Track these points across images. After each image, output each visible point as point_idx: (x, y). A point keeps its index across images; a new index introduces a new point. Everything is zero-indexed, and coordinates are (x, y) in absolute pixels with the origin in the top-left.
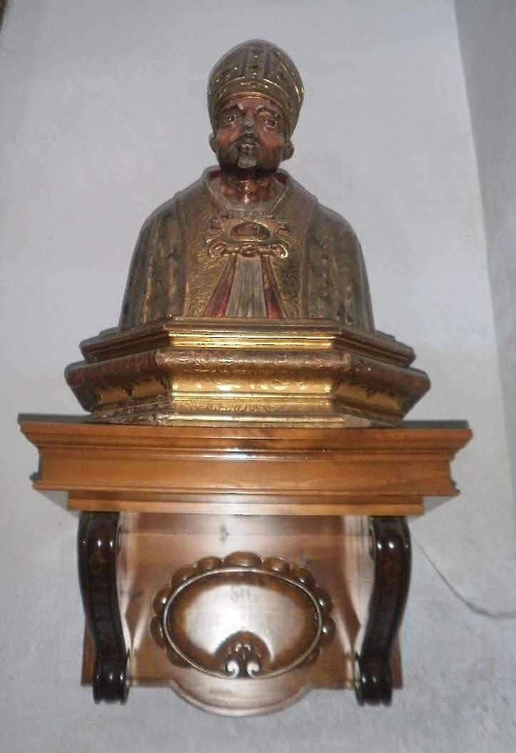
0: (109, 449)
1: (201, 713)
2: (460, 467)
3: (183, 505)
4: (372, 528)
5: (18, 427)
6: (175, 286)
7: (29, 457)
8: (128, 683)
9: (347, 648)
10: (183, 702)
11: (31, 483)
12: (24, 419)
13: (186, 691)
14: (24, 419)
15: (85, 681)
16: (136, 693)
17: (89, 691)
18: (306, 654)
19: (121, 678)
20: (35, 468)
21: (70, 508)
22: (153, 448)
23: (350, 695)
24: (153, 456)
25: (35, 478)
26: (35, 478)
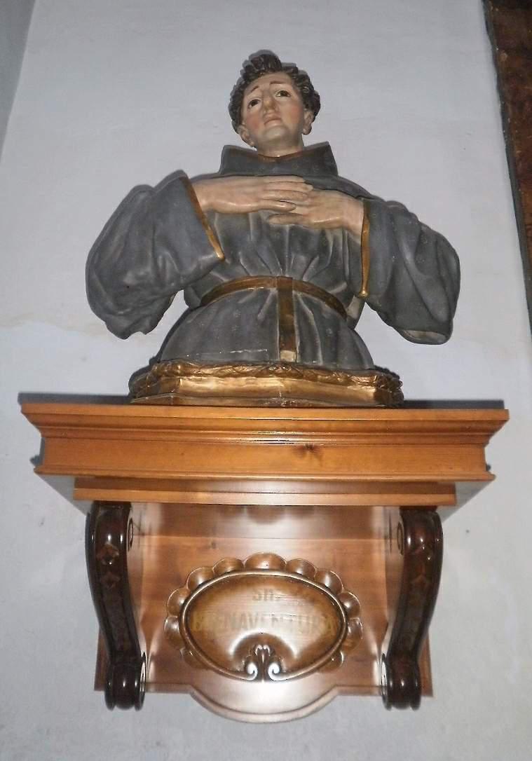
0: (182, 433)
1: (216, 717)
2: (496, 450)
3: (226, 495)
4: (401, 522)
5: (19, 408)
6: (278, 222)
7: (31, 440)
8: (142, 689)
9: (374, 649)
10: (210, 714)
11: (32, 467)
12: (25, 399)
13: (212, 702)
14: (25, 399)
15: (97, 687)
16: (152, 699)
17: (101, 695)
18: (328, 656)
19: (136, 684)
20: (36, 450)
21: (76, 500)
22: (477, 434)
23: (376, 701)
24: (147, 437)
25: (35, 461)
26: (35, 461)
